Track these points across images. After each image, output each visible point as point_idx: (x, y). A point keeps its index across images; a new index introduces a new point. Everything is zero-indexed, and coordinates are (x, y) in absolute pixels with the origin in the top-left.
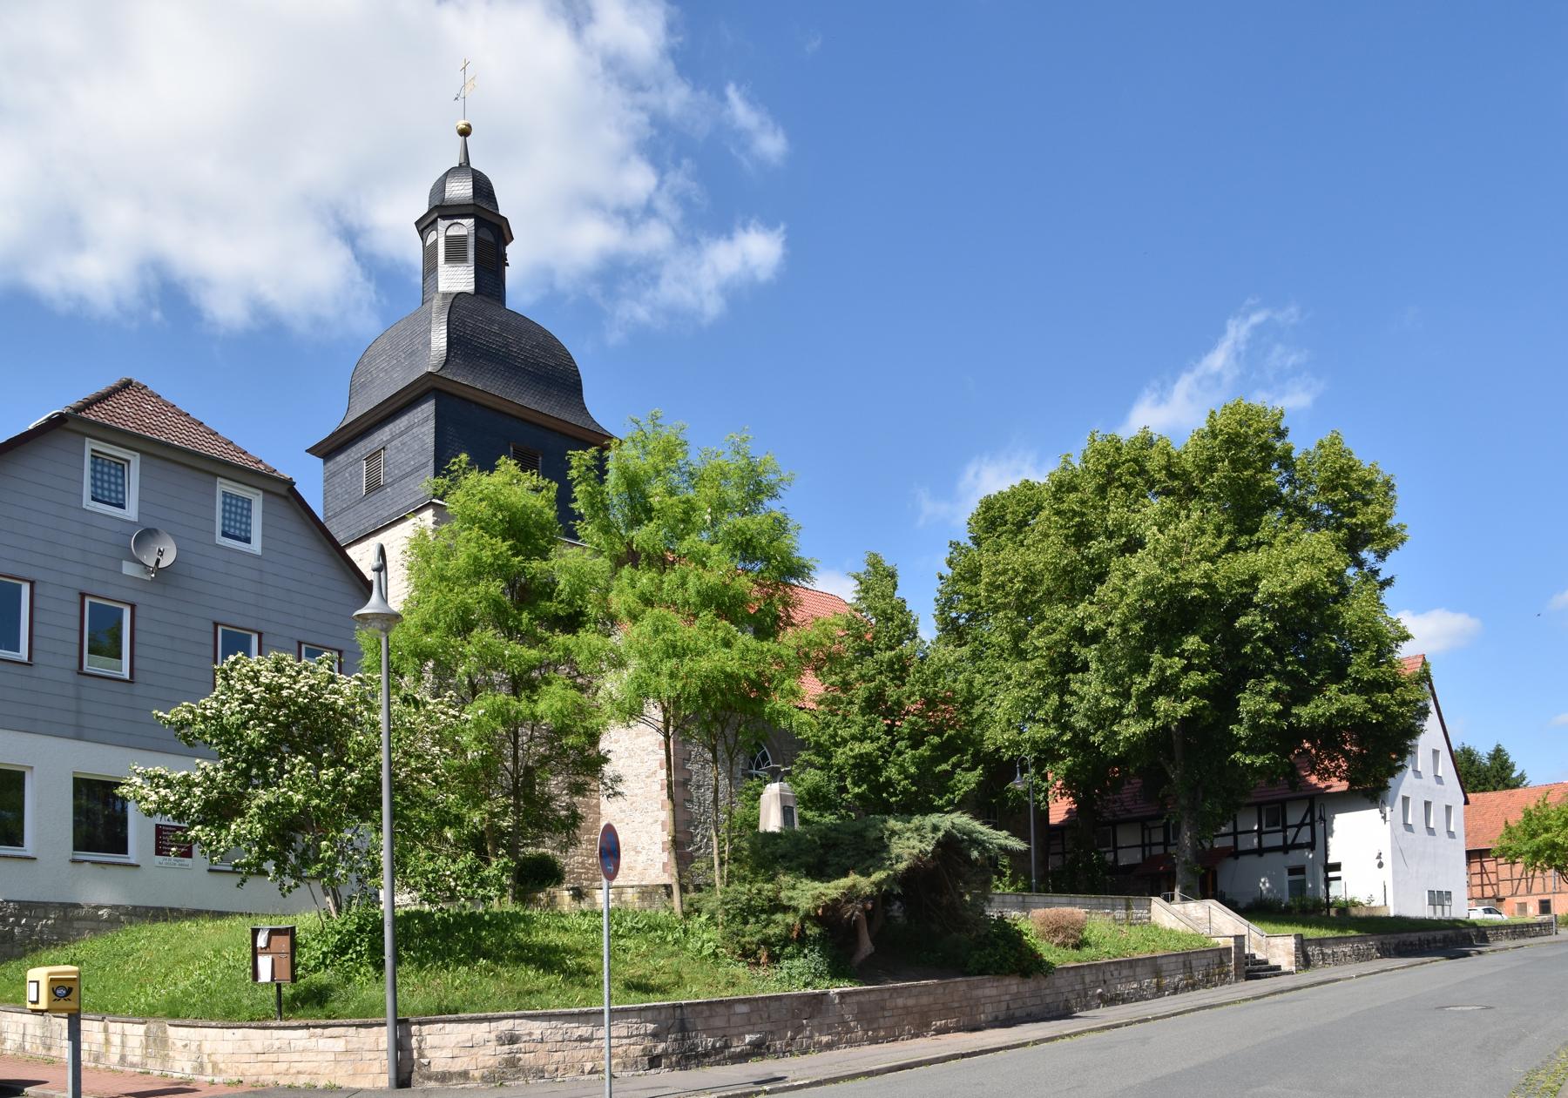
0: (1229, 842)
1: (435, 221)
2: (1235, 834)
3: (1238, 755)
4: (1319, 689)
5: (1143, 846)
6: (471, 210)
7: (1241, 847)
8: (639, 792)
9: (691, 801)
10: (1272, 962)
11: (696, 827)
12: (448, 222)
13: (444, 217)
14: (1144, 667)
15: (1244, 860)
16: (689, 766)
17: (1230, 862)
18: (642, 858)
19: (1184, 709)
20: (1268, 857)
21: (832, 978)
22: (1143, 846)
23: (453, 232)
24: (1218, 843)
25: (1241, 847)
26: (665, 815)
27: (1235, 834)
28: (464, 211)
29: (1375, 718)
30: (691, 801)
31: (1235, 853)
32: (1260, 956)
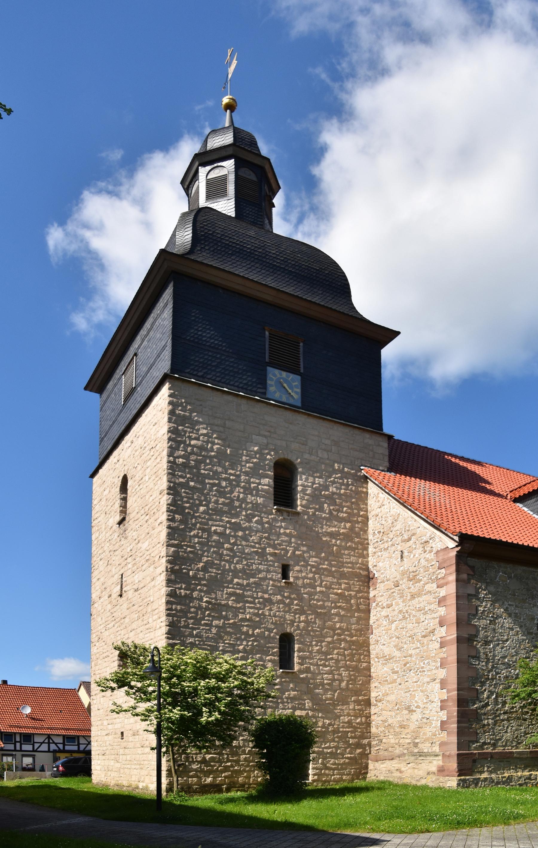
1: (197, 172)
6: (230, 151)
8: (413, 652)
9: (477, 658)
11: (483, 684)
12: (208, 168)
13: (204, 165)
16: (475, 622)
18: (416, 716)
20: (122, 714)
21: (390, 470)
23: (213, 175)
26: (451, 672)
28: (224, 153)
30: (477, 658)
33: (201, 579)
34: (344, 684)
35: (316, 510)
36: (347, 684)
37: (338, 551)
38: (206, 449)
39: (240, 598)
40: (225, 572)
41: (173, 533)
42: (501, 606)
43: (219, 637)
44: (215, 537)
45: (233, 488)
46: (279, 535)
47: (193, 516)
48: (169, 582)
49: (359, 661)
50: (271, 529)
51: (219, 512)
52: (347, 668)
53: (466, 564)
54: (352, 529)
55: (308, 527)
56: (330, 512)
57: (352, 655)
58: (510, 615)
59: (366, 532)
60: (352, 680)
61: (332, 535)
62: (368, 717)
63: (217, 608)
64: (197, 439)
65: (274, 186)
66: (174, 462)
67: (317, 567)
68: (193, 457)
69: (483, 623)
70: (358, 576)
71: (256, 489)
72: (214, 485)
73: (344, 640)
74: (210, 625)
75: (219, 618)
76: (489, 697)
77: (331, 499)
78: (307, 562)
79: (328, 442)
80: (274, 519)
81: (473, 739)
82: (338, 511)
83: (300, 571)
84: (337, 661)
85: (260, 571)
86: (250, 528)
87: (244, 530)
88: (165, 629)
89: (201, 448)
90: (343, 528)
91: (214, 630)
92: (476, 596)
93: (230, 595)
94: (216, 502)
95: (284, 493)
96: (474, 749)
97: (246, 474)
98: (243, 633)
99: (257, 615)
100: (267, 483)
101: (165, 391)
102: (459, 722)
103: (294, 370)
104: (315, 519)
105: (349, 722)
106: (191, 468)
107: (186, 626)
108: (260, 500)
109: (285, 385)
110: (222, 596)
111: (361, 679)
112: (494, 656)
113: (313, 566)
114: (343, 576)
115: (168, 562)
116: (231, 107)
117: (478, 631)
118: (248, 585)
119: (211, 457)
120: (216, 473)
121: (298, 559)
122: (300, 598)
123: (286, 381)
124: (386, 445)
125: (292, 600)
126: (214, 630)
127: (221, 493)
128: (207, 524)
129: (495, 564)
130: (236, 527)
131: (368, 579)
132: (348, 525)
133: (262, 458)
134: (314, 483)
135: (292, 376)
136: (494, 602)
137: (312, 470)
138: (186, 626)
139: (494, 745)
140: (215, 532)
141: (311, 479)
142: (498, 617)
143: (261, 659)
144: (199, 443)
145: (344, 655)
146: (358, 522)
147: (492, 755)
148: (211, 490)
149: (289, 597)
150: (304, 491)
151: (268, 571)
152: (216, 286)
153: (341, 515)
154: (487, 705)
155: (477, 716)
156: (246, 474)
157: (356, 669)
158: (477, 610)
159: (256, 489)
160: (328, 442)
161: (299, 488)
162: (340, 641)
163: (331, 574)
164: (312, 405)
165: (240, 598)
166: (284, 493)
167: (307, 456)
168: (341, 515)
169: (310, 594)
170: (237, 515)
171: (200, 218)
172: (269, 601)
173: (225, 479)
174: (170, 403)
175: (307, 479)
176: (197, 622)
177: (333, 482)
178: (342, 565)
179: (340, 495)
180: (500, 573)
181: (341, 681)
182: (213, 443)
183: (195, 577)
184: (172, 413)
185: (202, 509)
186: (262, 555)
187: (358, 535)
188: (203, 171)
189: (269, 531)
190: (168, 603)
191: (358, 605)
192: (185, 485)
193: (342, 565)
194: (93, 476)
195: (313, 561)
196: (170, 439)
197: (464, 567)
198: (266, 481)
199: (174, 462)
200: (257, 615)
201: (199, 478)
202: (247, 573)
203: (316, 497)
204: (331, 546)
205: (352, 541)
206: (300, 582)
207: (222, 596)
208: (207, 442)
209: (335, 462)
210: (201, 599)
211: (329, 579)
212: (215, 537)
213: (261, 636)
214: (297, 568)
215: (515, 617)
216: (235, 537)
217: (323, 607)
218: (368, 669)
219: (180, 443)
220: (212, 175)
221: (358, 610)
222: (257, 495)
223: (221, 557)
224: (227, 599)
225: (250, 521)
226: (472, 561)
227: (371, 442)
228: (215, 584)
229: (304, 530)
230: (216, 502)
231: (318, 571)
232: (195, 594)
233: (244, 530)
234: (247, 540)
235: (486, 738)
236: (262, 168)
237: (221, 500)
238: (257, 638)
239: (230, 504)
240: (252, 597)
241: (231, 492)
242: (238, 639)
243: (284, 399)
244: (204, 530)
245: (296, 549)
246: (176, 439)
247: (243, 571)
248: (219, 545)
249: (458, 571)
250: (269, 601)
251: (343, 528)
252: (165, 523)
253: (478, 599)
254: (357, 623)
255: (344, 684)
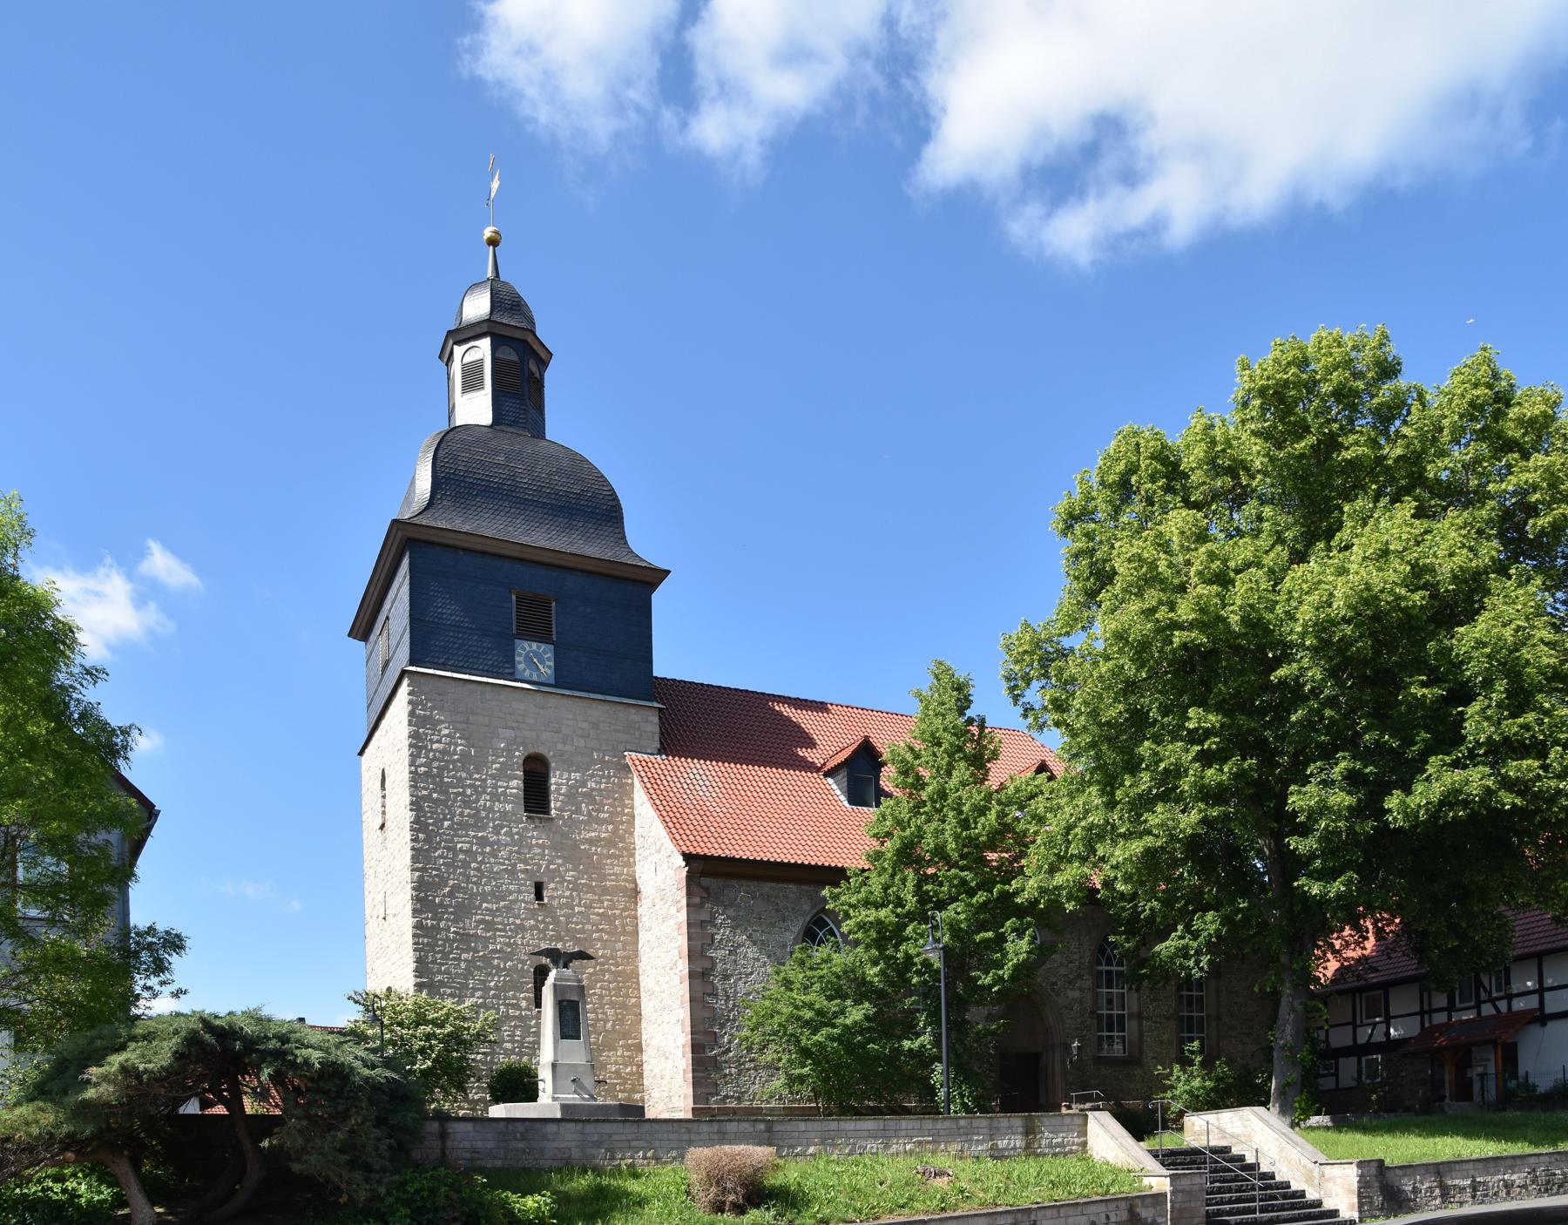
0: (1531, 1003)
2: (1541, 991)
3: (1303, 880)
4: (1418, 765)
5: (1421, 1013)
6: (485, 328)
7: (1549, 1009)
9: (714, 995)
10: (1328, 1205)
11: (722, 1026)
14: (1133, 766)
15: (1550, 1024)
17: (1536, 1029)
19: (1189, 820)
22: (1421, 1013)
24: (1519, 1005)
25: (1549, 1009)
27: (1541, 991)
28: (479, 331)
29: (1508, 799)
30: (714, 995)
31: (1541, 1018)
32: (1311, 1195)
33: (447, 907)
34: (609, 1025)
35: (573, 812)
36: (614, 1026)
37: (600, 861)
38: (448, 753)
39: (490, 926)
40: (472, 896)
41: (417, 855)
42: (742, 933)
43: (468, 973)
44: (461, 856)
45: (479, 795)
46: (531, 847)
47: (438, 834)
48: (415, 912)
49: (627, 996)
50: (521, 842)
51: (464, 826)
52: (613, 1005)
53: (699, 885)
54: (615, 832)
55: (563, 834)
56: (589, 815)
57: (619, 989)
58: (755, 943)
59: (632, 834)
60: (619, 1020)
61: (591, 842)
62: (640, 1065)
63: (464, 938)
64: (439, 742)
65: (543, 355)
66: (416, 773)
67: (574, 883)
68: (436, 764)
69: (721, 953)
70: (623, 890)
71: (504, 793)
72: (458, 794)
73: (609, 970)
74: (458, 959)
75: (467, 951)
76: (730, 1042)
77: (589, 796)
78: (563, 877)
79: (585, 725)
80: (525, 829)
81: (713, 1090)
82: (598, 811)
83: (556, 889)
84: (601, 997)
85: (511, 893)
86: (498, 842)
87: (491, 844)
88: (413, 966)
89: (444, 752)
90: (604, 832)
91: (463, 965)
92: (712, 922)
93: (480, 922)
94: (461, 814)
95: (536, 796)
96: (714, 1102)
97: (493, 777)
98: (494, 967)
99: (509, 944)
100: (516, 785)
101: (404, 688)
102: (694, 1071)
103: (544, 638)
104: (571, 823)
105: (617, 1072)
106: (433, 777)
107: (434, 962)
108: (509, 807)
109: (535, 658)
110: (471, 925)
111: (630, 1019)
112: (736, 992)
113: (569, 882)
114: (605, 891)
115: (414, 889)
116: (493, 242)
117: (714, 964)
118: (498, 909)
119: (454, 762)
120: (460, 779)
121: (554, 874)
122: (556, 922)
123: (537, 655)
124: (656, 719)
125: (548, 924)
126: (463, 965)
127: (467, 803)
128: (452, 841)
129: (734, 882)
130: (483, 842)
131: (635, 893)
132: (610, 827)
133: (510, 756)
134: (569, 779)
135: (543, 646)
136: (733, 928)
137: (569, 766)
138: (434, 962)
139: (739, 1099)
140: (461, 850)
141: (566, 775)
142: (739, 946)
143: (514, 997)
144: (441, 746)
145: (608, 989)
146: (622, 823)
147: (734, 1111)
148: (455, 801)
149: (543, 922)
150: (557, 790)
151: (519, 892)
152: (456, 548)
153: (602, 815)
154: (729, 1050)
155: (715, 1064)
156: (493, 777)
157: (623, 1006)
158: (713, 939)
159: (504, 793)
160: (585, 725)
161: (553, 788)
162: (603, 972)
163: (591, 889)
164: (567, 679)
165: (490, 926)
166: (536, 796)
167: (560, 746)
168: (602, 815)
169: (568, 916)
170: (484, 828)
171: (441, 453)
172: (521, 928)
173: (470, 786)
174: (410, 702)
175: (561, 777)
176: (445, 956)
177: (592, 776)
178: (603, 877)
179: (600, 790)
180: (742, 893)
181: (606, 1021)
182: (456, 745)
183: (441, 905)
184: (412, 714)
185: (446, 824)
186: (512, 872)
187: (623, 840)
188: (458, 351)
189: (519, 843)
190: (414, 936)
191: (623, 926)
192: (428, 798)
193: (603, 877)
194: (361, 753)
195: (570, 875)
196: (411, 746)
197: (697, 890)
198: (514, 783)
199: (416, 773)
200: (509, 944)
201: (443, 788)
202: (498, 896)
203: (572, 796)
204: (590, 856)
205: (615, 846)
206: (555, 903)
207: (471, 925)
208: (450, 744)
209: (593, 749)
210: (448, 930)
211: (589, 896)
212: (461, 856)
213: (514, 969)
214: (552, 886)
215: (763, 946)
216: (483, 853)
217: (582, 931)
218: (639, 1005)
219: (421, 748)
220: (467, 359)
221: (624, 933)
222: (506, 801)
223: (467, 878)
224: (476, 928)
225: (498, 834)
226: (706, 881)
227: (637, 718)
228: (463, 911)
229: (558, 838)
230: (461, 814)
231: (576, 887)
232: (442, 924)
233: (491, 844)
234: (496, 857)
235: (728, 1090)
236: (525, 342)
237: (467, 811)
238: (509, 972)
239: (476, 815)
240: (502, 923)
241: (477, 800)
242: (489, 974)
243: (535, 678)
244: (449, 849)
245: (550, 862)
246: (418, 743)
247: (492, 893)
248: (466, 865)
249: (689, 894)
250: (521, 928)
251: (604, 832)
252: (410, 845)
253: (715, 926)
254: (624, 949)
255: (609, 1025)
